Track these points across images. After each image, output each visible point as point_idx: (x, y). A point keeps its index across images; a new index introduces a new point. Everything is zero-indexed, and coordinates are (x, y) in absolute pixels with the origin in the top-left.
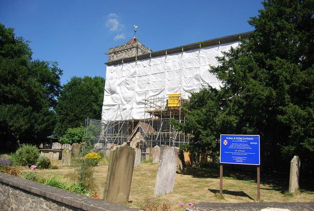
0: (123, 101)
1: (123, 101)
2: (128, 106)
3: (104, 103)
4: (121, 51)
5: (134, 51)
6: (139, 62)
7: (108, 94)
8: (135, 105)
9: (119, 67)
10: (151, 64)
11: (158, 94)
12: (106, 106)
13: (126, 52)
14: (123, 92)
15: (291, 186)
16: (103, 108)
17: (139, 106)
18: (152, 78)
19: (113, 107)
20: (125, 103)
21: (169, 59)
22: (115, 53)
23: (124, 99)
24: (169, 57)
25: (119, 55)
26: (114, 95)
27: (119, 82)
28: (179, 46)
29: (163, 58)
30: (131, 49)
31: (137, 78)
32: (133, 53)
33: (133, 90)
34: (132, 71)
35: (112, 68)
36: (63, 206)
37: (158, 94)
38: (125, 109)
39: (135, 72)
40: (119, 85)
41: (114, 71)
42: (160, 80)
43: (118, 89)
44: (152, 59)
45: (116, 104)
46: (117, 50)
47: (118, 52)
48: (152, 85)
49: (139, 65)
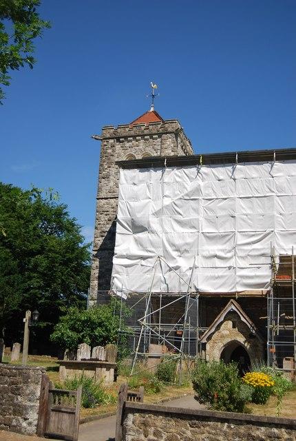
0: (169, 249)
1: (169, 249)
2: (183, 263)
3: (117, 250)
4: (134, 137)
5: (169, 141)
6: (204, 169)
7: (128, 233)
8: (200, 262)
9: (155, 175)
10: (238, 175)
11: (254, 243)
12: (122, 257)
13: (147, 140)
14: (167, 231)
15: (181, 409)
16: (115, 261)
17: (209, 263)
18: (243, 208)
19: (143, 262)
20: (175, 254)
21: (279, 171)
22: (118, 139)
23: (172, 245)
24: (277, 165)
25: (127, 145)
26: (142, 236)
27: (154, 206)
28: (269, 148)
29: (267, 166)
30: (160, 135)
31: (203, 204)
32: (169, 148)
33: (194, 227)
34: (190, 186)
35: (135, 173)
36: (225, 422)
37: (254, 243)
38: (177, 268)
39: (198, 190)
40: (156, 214)
41: (141, 182)
42: (260, 211)
43: (155, 224)
44: (238, 166)
45: (150, 254)
46: (121, 132)
47: (126, 138)
48: (241, 222)
49: (205, 174)
